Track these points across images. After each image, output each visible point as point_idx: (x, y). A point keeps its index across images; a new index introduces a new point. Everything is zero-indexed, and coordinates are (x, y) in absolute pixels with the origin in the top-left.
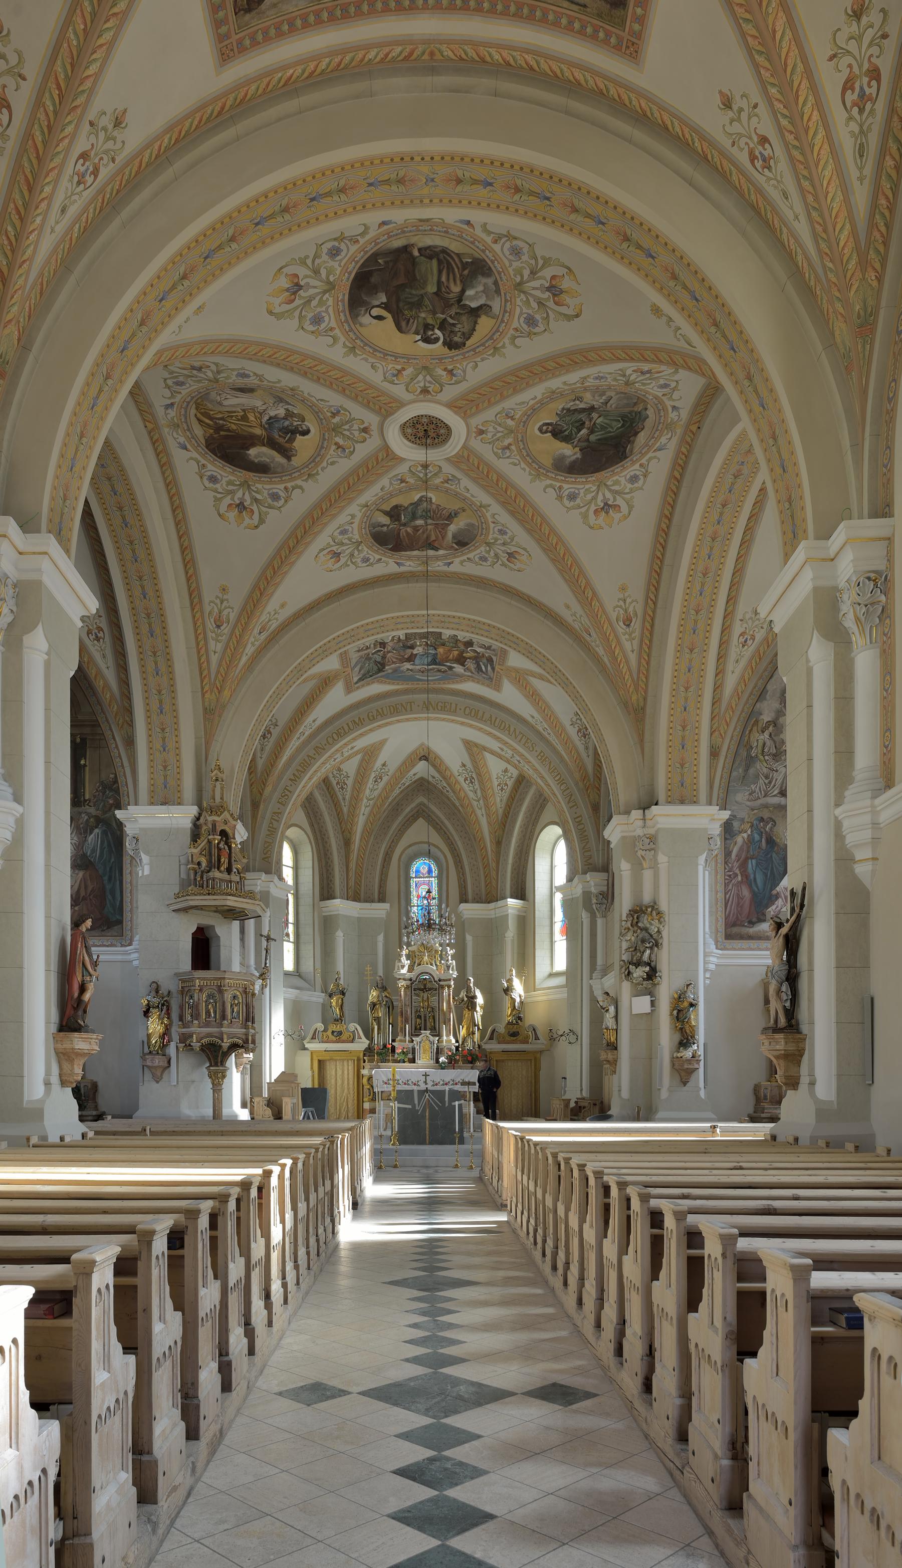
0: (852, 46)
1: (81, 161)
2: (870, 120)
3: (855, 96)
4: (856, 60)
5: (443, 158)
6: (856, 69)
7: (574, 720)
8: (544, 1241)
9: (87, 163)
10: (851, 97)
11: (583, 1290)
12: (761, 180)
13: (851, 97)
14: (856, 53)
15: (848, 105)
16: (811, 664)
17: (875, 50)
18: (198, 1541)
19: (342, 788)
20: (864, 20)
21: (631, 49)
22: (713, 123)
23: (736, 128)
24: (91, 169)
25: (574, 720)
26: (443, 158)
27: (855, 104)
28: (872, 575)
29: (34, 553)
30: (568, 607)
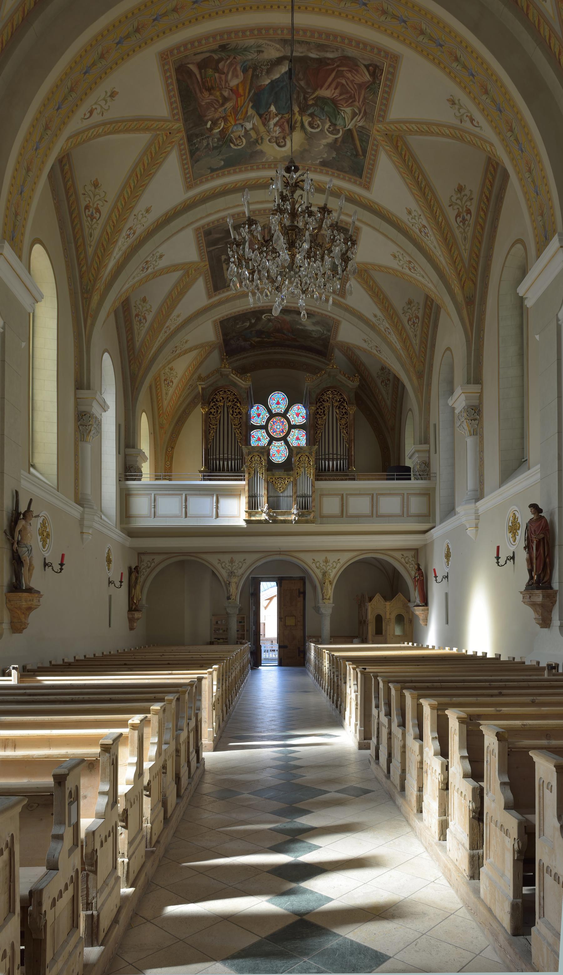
0: (459, 202)
1: (87, 211)
2: (468, 228)
3: (461, 219)
4: (459, 205)
5: (272, 7)
6: (461, 210)
7: (454, 199)
8: (389, 761)
9: (91, 209)
10: (459, 219)
11: (448, 831)
12: (414, 275)
13: (459, 219)
14: (460, 204)
15: (458, 222)
16: (560, 322)
17: (468, 203)
18: (130, 964)
19: (92, 217)
20: (463, 193)
21: (367, 187)
22: (404, 217)
23: (402, 262)
24: (94, 211)
25: (454, 199)
26: (272, 7)
27: (461, 222)
28: (474, 408)
29: (186, 508)
30: (375, 316)
